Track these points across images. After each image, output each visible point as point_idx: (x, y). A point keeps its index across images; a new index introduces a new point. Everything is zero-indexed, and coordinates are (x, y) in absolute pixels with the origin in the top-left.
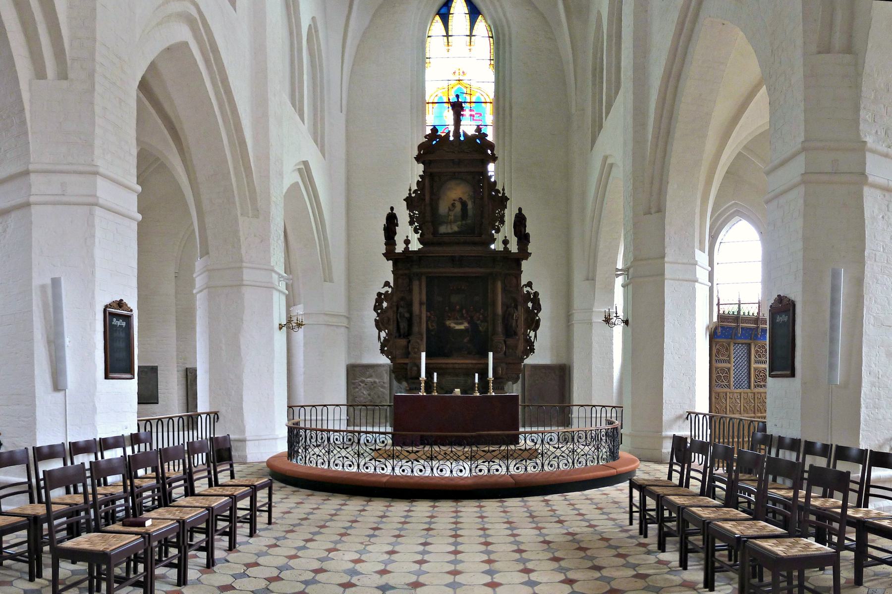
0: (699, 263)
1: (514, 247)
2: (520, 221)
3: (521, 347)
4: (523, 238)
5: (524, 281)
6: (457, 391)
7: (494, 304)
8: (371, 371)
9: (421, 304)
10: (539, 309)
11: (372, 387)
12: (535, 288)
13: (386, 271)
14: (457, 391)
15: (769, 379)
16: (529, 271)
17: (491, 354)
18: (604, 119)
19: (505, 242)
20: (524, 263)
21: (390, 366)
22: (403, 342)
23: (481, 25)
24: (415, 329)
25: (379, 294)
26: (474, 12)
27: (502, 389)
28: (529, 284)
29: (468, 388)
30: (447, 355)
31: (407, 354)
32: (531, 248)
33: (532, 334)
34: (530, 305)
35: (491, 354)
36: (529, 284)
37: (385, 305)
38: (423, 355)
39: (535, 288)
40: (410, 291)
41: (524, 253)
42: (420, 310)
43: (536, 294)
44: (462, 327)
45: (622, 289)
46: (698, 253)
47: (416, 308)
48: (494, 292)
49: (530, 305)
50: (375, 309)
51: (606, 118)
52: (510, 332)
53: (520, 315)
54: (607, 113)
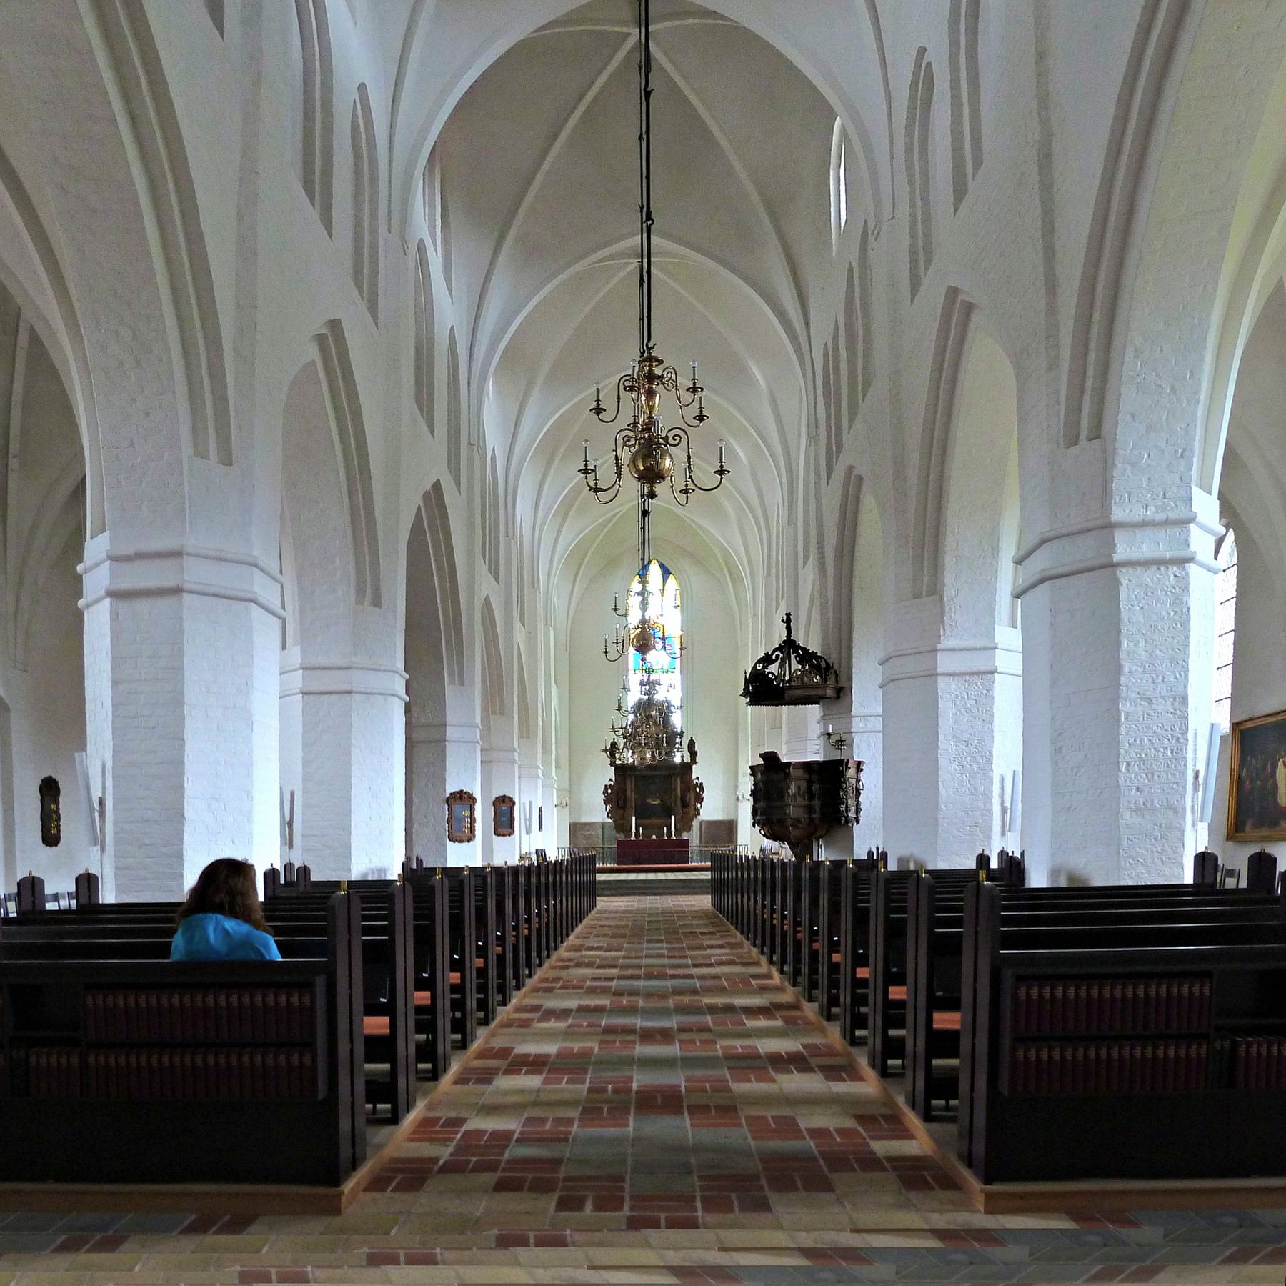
0: (1200, 518)
1: (688, 759)
2: (691, 744)
3: (692, 812)
4: (693, 754)
5: (694, 777)
6: (654, 837)
7: (675, 789)
8: (588, 827)
9: (632, 790)
10: (703, 792)
11: (589, 838)
12: (701, 780)
13: (610, 773)
14: (654, 837)
15: (449, 844)
16: (696, 772)
17: (673, 817)
18: (860, 395)
19: (682, 757)
20: (694, 766)
21: (603, 825)
22: (621, 812)
23: (672, 581)
24: (628, 804)
25: (606, 786)
26: (666, 572)
27: (681, 835)
28: (698, 778)
29: (660, 835)
30: (649, 817)
31: (623, 817)
32: (697, 759)
33: (699, 806)
34: (698, 789)
35: (673, 817)
36: (698, 778)
37: (609, 791)
38: (634, 818)
39: (701, 780)
40: (625, 783)
41: (694, 761)
42: (631, 794)
43: (701, 784)
44: (656, 803)
45: (1011, 565)
46: (1197, 493)
47: (629, 792)
48: (676, 783)
49: (698, 789)
50: (604, 794)
51: (850, 428)
52: (685, 805)
53: (692, 795)
54: (838, 457)
